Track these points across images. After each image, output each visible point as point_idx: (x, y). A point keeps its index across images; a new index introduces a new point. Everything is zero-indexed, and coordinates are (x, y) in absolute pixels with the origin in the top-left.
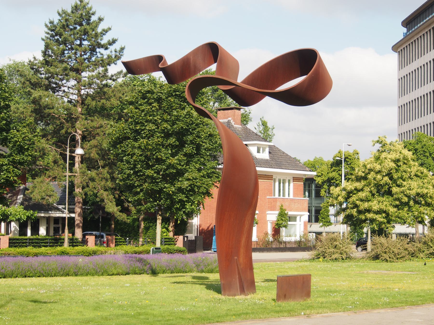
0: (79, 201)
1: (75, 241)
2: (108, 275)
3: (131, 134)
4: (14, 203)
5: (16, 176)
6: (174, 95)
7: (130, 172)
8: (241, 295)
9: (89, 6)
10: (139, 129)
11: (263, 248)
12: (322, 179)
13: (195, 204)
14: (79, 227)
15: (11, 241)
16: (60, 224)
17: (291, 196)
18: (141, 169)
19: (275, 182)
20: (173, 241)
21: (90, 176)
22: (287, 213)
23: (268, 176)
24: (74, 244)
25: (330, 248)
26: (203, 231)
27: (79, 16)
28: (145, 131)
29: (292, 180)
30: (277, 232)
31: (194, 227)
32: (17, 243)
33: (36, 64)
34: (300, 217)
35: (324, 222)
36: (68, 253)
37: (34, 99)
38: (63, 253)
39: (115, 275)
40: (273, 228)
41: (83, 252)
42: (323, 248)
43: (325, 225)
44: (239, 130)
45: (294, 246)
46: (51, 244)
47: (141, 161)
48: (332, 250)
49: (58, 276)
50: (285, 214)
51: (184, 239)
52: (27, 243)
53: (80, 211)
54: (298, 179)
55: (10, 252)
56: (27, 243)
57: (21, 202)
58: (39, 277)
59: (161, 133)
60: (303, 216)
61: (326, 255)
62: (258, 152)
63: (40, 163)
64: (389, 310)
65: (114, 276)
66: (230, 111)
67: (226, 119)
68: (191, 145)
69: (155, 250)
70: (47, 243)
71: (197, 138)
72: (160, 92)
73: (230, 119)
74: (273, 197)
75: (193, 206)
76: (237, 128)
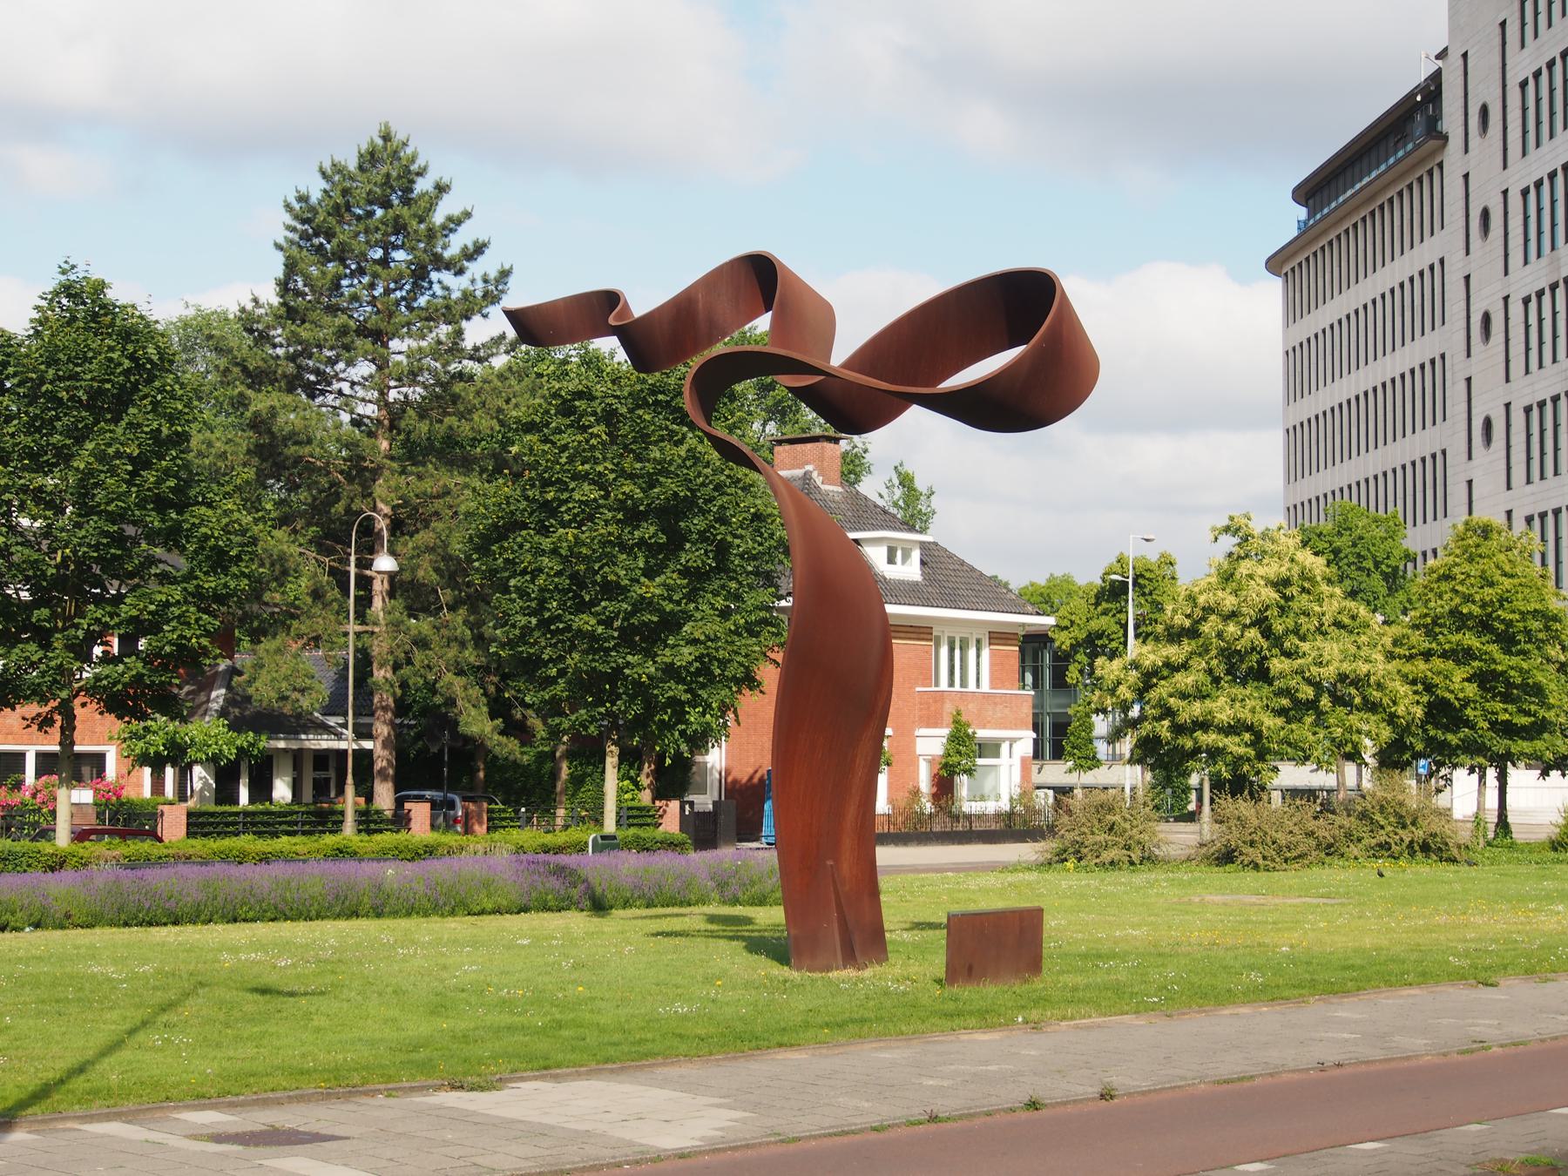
1: (375, 817)
4: (201, 711)
10: (554, 499)
14: (385, 778)
15: (193, 820)
17: (985, 687)
19: (938, 646)
22: (974, 733)
24: (372, 826)
28: (570, 505)
30: (944, 786)
32: (211, 824)
33: (260, 317)
34: (1011, 746)
38: (341, 853)
42: (1077, 832)
46: (307, 828)
47: (559, 591)
48: (1102, 837)
50: (968, 736)
51: (682, 809)
59: (615, 510)
61: (1084, 851)
62: (891, 560)
63: (273, 598)
66: (809, 446)
69: (600, 840)
73: (809, 468)
74: (934, 689)
75: (708, 716)
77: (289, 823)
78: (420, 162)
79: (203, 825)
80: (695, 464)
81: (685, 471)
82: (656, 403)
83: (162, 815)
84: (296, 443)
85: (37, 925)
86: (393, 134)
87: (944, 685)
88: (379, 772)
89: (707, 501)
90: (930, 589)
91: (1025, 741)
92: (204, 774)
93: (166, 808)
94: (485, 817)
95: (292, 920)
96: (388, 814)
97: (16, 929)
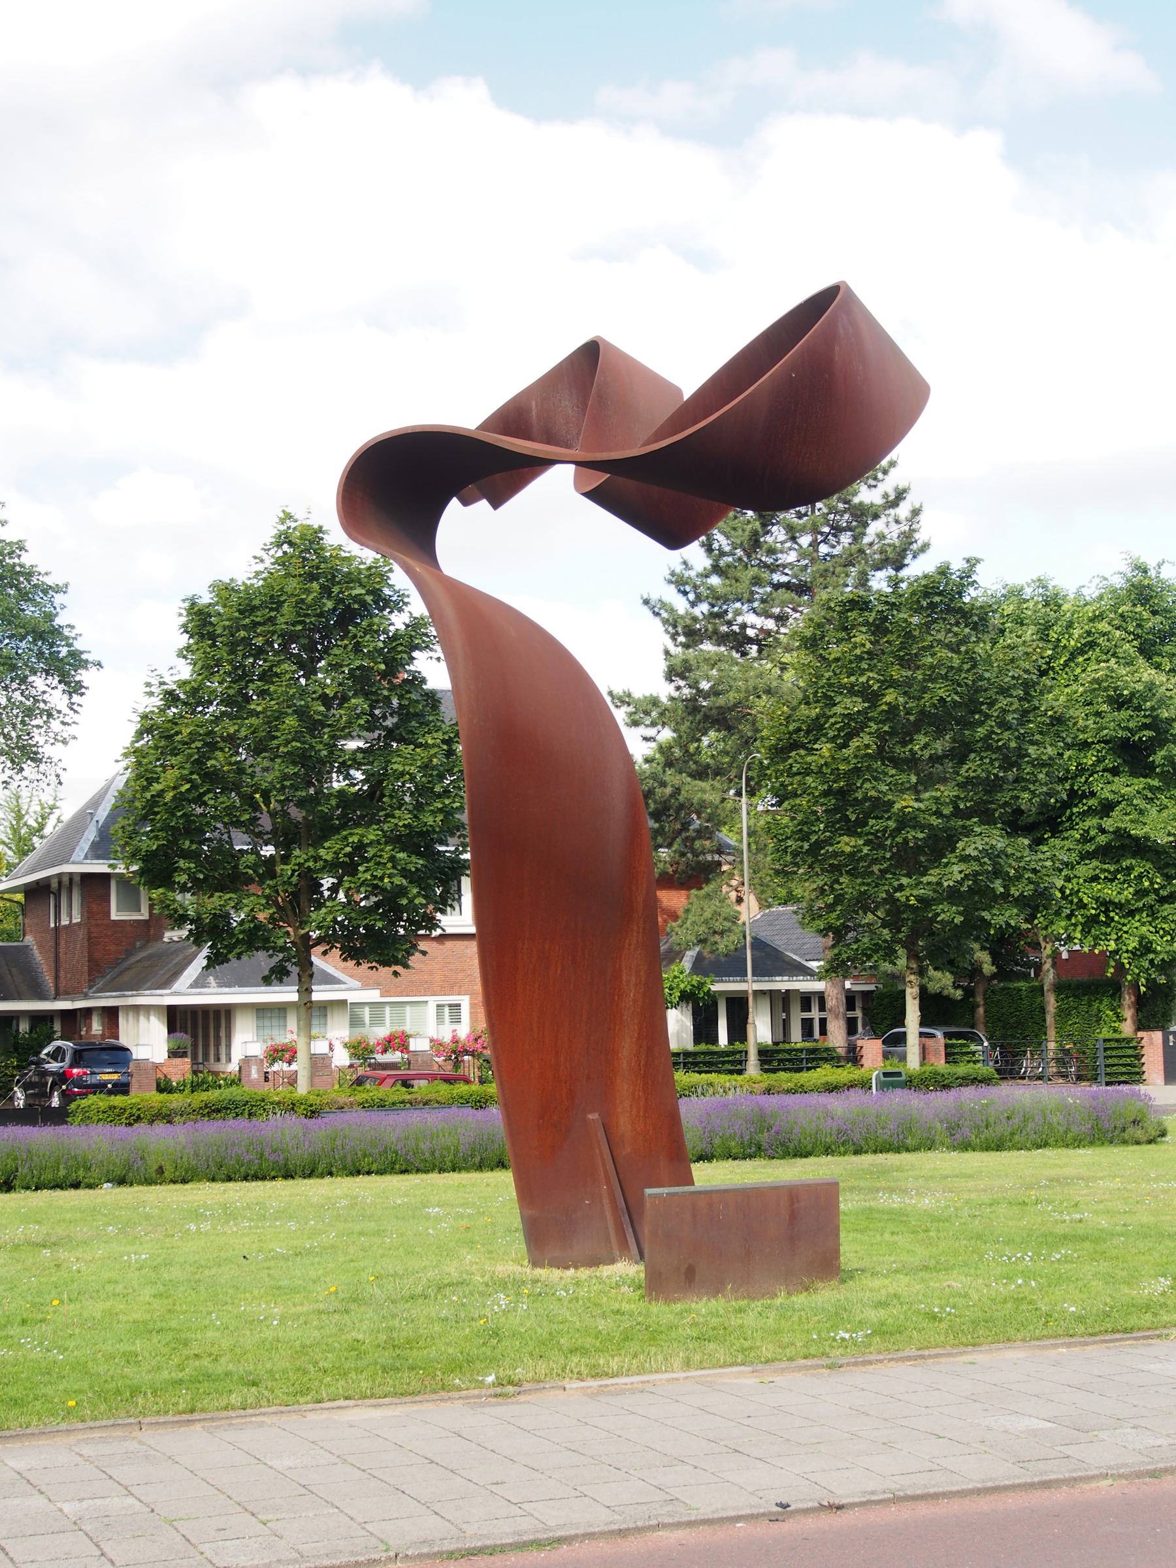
1: (825, 1055)
5: (405, 873)
51: (1165, 1041)
59: (880, 722)
63: (702, 846)
68: (985, 751)
69: (882, 1079)
77: (732, 1062)
82: (932, 606)
85: (121, 1181)
94: (943, 1053)
96: (841, 1052)
97: (90, 1186)
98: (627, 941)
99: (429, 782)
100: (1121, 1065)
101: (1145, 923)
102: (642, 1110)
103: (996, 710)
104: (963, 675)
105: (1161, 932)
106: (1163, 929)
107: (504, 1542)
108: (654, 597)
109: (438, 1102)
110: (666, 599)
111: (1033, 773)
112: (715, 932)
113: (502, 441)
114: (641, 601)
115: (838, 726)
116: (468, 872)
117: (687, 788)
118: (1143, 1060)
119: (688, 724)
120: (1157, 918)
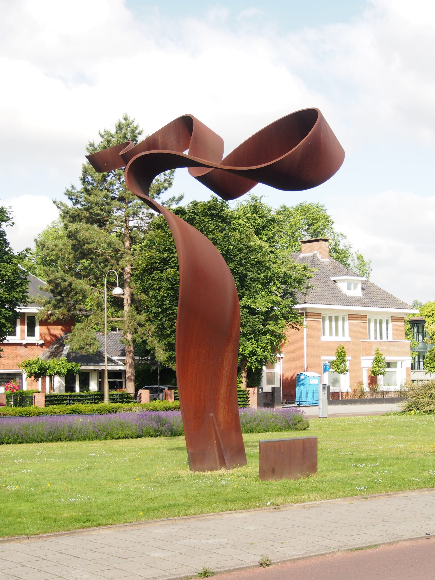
0: (129, 350)
1: (126, 396)
2: (113, 439)
3: (160, 263)
4: (59, 355)
6: (209, 214)
7: (158, 310)
8: (221, 469)
9: (135, 124)
10: (167, 257)
11: (356, 400)
12: (432, 319)
13: (268, 350)
14: (131, 380)
15: (48, 399)
16: (123, 377)
17: (390, 339)
18: (170, 305)
19: (369, 322)
20: (246, 394)
21: (139, 320)
22: (384, 358)
23: (361, 316)
24: (125, 400)
25: (424, 397)
26: (287, 381)
27: (122, 136)
28: (173, 259)
29: (390, 320)
30: (373, 380)
31: (277, 377)
32: (56, 400)
33: (75, 193)
34: (401, 363)
35: (430, 368)
36: (81, 412)
37: (70, 233)
38: (101, 412)
39: (123, 438)
40: (369, 376)
41: (100, 409)
42: (416, 398)
43: (431, 371)
44: (327, 264)
45: (393, 397)
46: (97, 401)
47: (170, 297)
48: (427, 400)
49: (44, 442)
50: (382, 359)
51: (258, 391)
52: (67, 400)
53: (131, 362)
54: (398, 318)
55: (7, 412)
56: (67, 400)
57: (68, 353)
58: (20, 443)
60: (405, 362)
61: (419, 406)
62: (349, 288)
64: (427, 491)
65: (120, 440)
66: (315, 243)
67: (312, 252)
70: (92, 400)
71: (239, 267)
72: (193, 212)
73: (316, 252)
74: (368, 340)
75: (266, 352)
76: (324, 262)
78: (140, 129)
79: (52, 401)
80: (228, 240)
81: (224, 243)
83: (35, 397)
84: (88, 243)
86: (128, 118)
87: (373, 338)
88: (128, 378)
89: (235, 256)
90: (366, 300)
91: (408, 361)
92: (60, 380)
93: (36, 394)
94: (173, 396)
95: (29, 443)
96: (132, 395)
98: (227, 349)
99: (14, 279)
100: (241, 401)
101: (253, 343)
102: (227, 412)
103: (237, 258)
104: (224, 243)
105: (260, 347)
106: (261, 346)
107: (362, 546)
108: (58, 200)
109: (10, 415)
110: (63, 202)
111: (251, 284)
112: (87, 344)
113: (197, 159)
114: (53, 202)
115: (176, 262)
116: (19, 317)
117: (75, 282)
118: (249, 400)
119: (73, 255)
120: (259, 341)
